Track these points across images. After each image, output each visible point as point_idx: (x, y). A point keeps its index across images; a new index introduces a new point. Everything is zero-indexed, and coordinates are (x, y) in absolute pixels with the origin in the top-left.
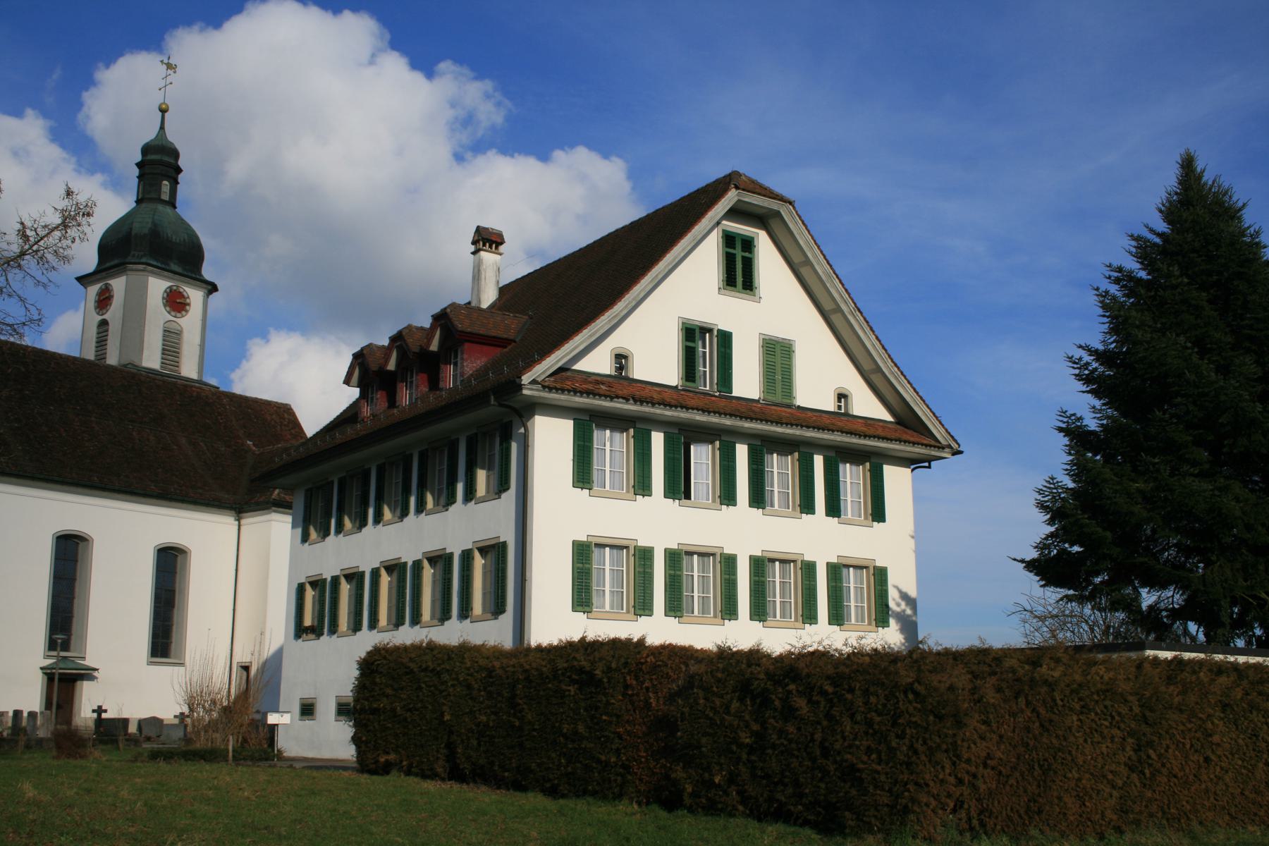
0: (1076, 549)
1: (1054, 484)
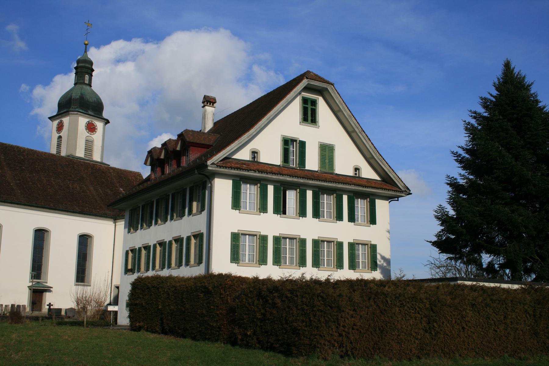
0: (453, 237)
1: (441, 208)
